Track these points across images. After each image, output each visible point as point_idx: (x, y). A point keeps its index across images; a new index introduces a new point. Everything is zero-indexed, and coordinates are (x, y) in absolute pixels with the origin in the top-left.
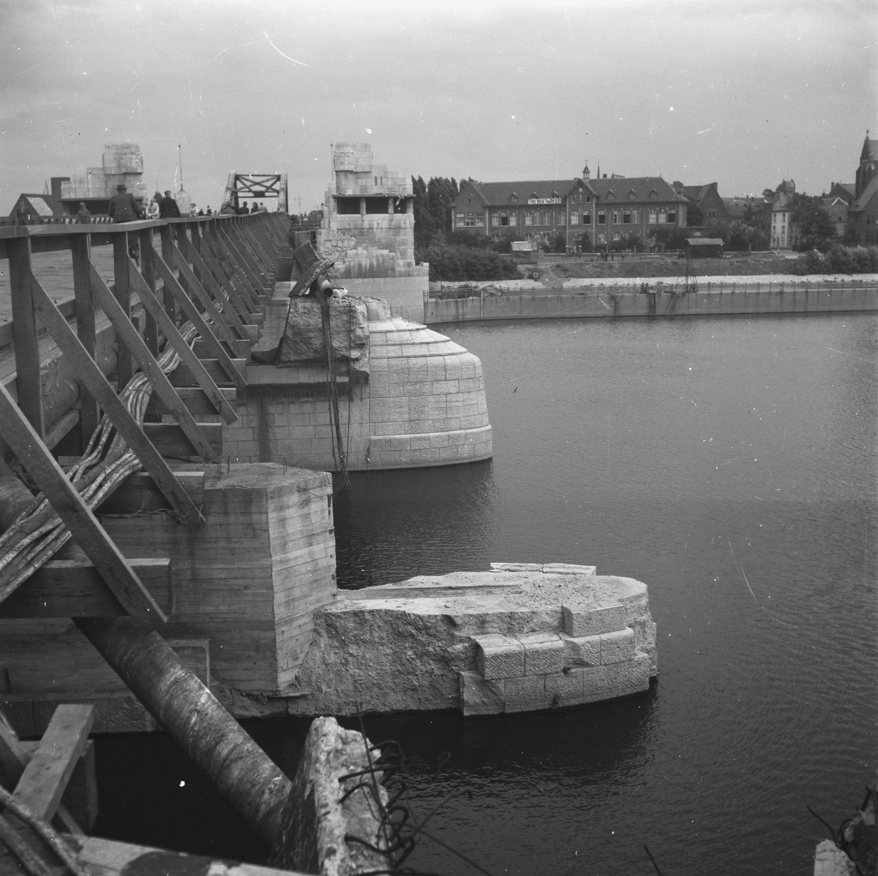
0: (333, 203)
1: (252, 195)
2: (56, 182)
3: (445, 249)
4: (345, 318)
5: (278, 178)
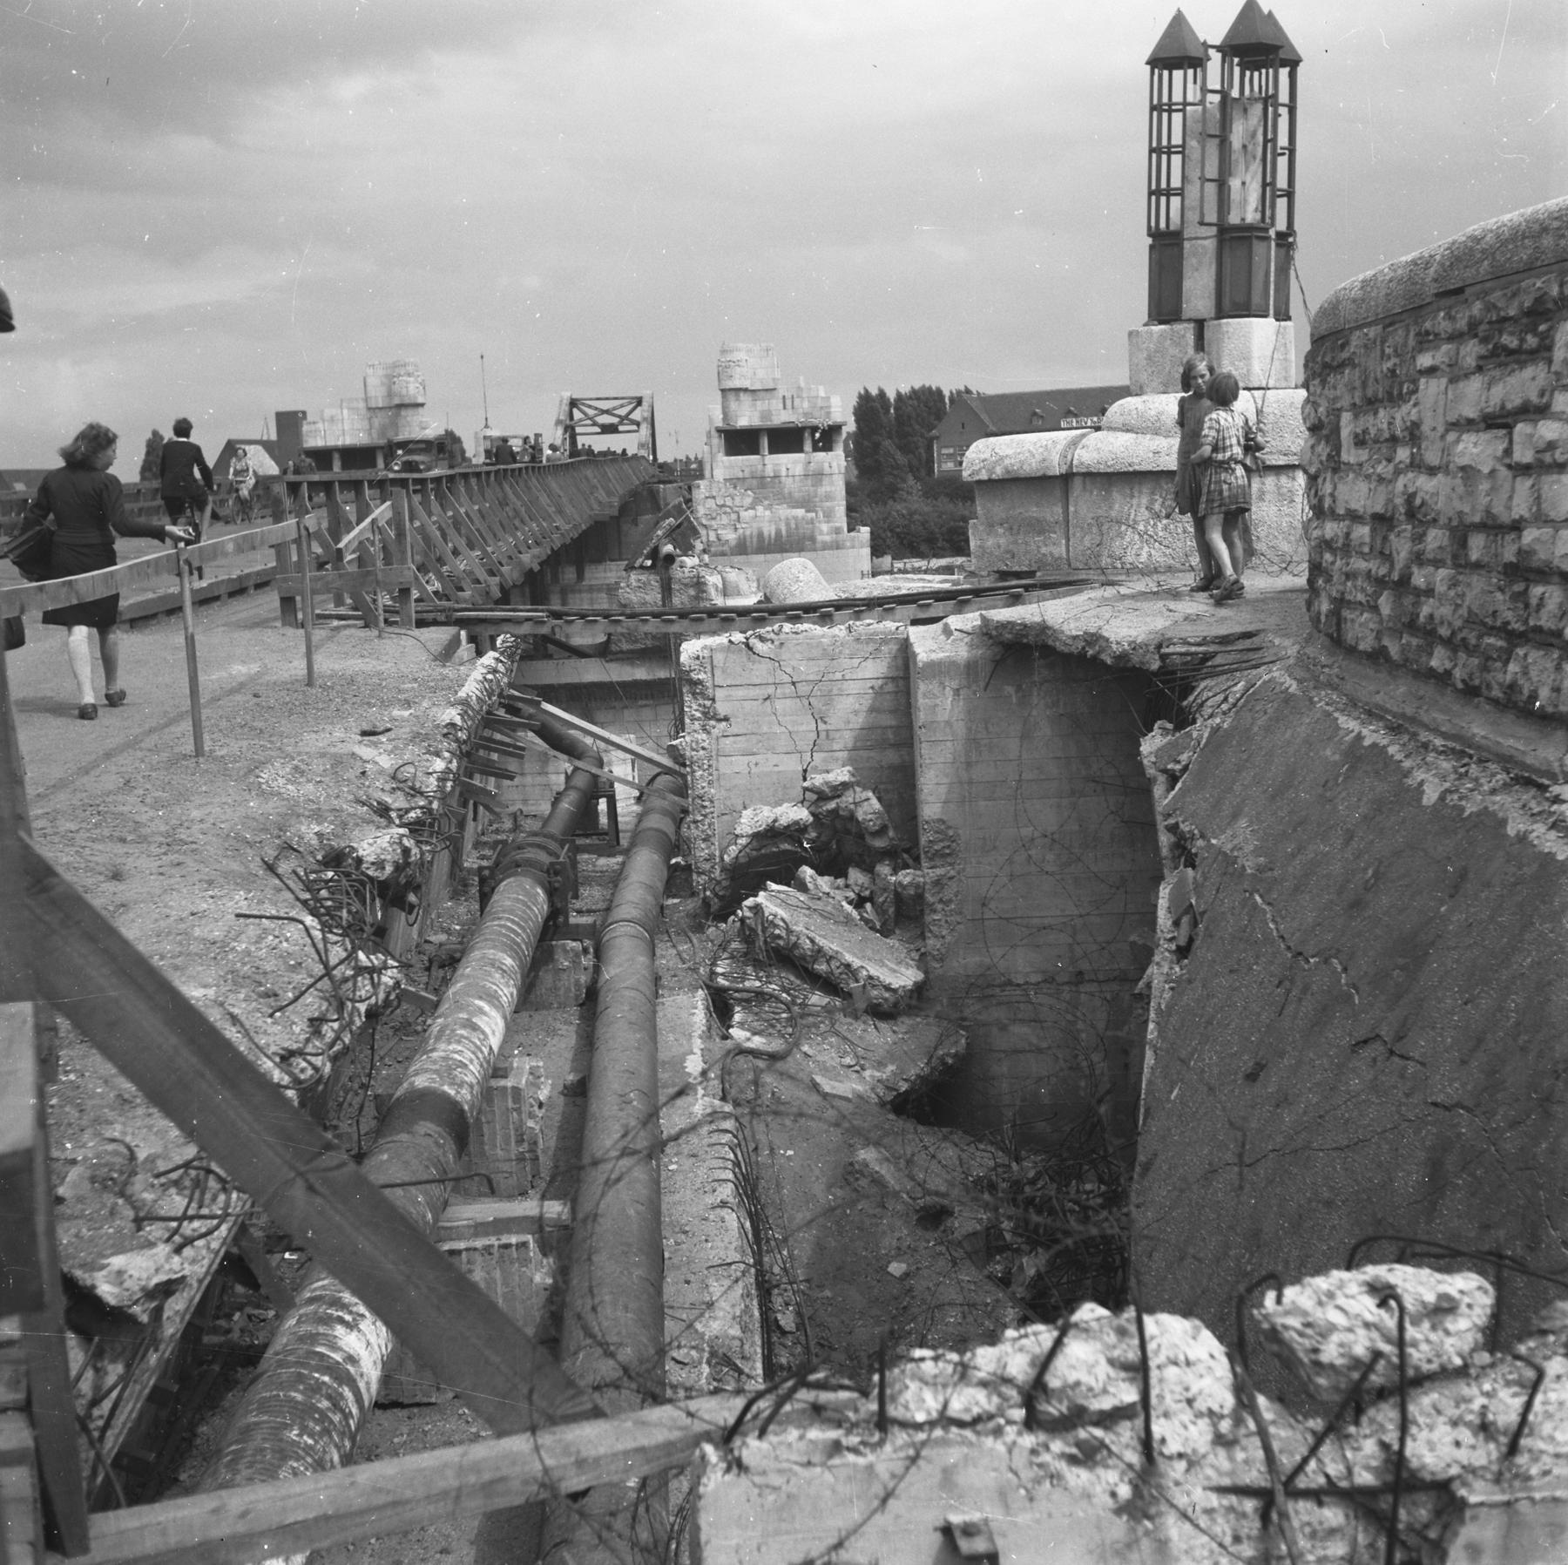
0: (718, 442)
1: (598, 429)
2: (289, 422)
3: (916, 506)
4: (692, 592)
5: (639, 402)
